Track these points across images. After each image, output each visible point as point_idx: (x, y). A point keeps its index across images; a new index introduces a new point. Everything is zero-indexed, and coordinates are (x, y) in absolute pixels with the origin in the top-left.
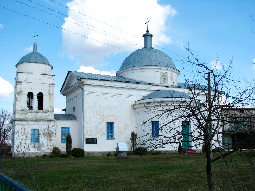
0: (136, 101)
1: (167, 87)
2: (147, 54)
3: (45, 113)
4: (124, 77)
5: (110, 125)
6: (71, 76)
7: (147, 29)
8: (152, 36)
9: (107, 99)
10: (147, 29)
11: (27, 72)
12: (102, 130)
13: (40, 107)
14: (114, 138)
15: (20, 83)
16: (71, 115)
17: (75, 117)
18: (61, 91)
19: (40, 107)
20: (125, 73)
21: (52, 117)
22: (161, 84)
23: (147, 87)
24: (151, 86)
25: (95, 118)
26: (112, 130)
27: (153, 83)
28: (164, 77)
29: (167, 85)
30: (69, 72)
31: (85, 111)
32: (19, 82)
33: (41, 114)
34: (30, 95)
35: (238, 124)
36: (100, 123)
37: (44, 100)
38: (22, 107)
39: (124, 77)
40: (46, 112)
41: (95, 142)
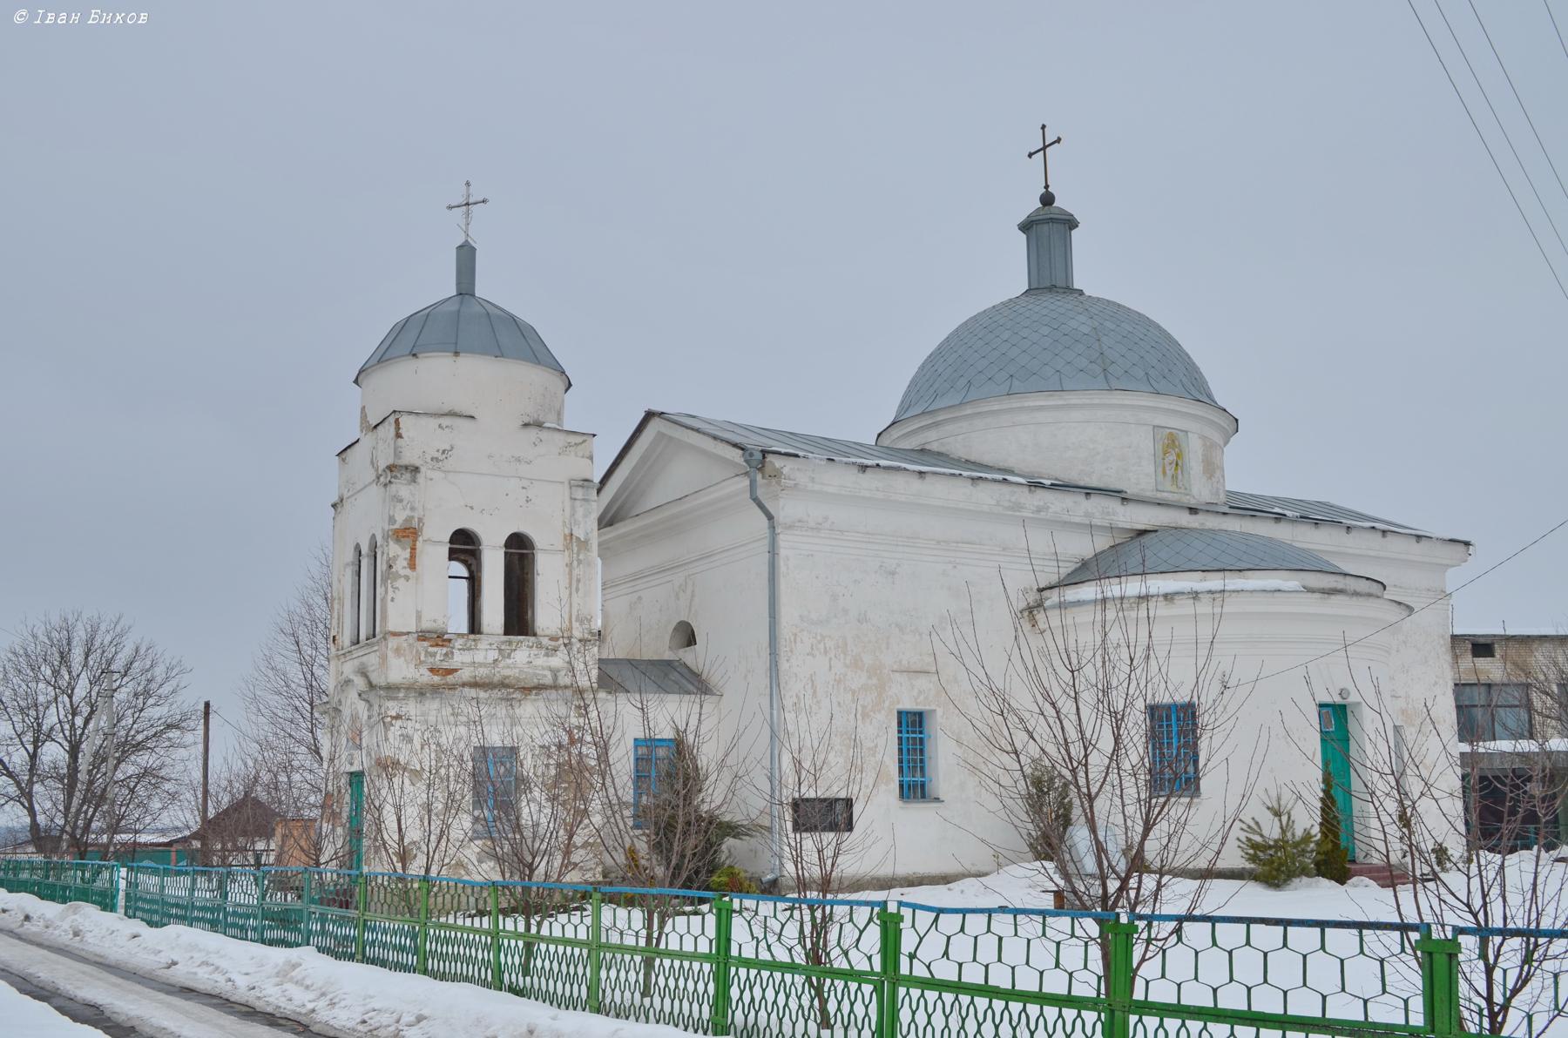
0: (1041, 590)
1: (1193, 511)
2: (1073, 324)
3: (547, 655)
4: (942, 450)
5: (913, 725)
7: (1047, 187)
8: (1071, 223)
9: (893, 573)
10: (1047, 187)
11: (446, 409)
13: (518, 620)
14: (937, 800)
15: (408, 476)
17: (697, 676)
19: (518, 620)
20: (949, 428)
22: (1159, 495)
23: (1097, 504)
24: (1113, 505)
25: (839, 682)
29: (1193, 503)
30: (649, 415)
31: (783, 642)
32: (406, 468)
33: (524, 658)
35: (441, 926)
38: (419, 617)
39: (939, 454)
41: (841, 819)
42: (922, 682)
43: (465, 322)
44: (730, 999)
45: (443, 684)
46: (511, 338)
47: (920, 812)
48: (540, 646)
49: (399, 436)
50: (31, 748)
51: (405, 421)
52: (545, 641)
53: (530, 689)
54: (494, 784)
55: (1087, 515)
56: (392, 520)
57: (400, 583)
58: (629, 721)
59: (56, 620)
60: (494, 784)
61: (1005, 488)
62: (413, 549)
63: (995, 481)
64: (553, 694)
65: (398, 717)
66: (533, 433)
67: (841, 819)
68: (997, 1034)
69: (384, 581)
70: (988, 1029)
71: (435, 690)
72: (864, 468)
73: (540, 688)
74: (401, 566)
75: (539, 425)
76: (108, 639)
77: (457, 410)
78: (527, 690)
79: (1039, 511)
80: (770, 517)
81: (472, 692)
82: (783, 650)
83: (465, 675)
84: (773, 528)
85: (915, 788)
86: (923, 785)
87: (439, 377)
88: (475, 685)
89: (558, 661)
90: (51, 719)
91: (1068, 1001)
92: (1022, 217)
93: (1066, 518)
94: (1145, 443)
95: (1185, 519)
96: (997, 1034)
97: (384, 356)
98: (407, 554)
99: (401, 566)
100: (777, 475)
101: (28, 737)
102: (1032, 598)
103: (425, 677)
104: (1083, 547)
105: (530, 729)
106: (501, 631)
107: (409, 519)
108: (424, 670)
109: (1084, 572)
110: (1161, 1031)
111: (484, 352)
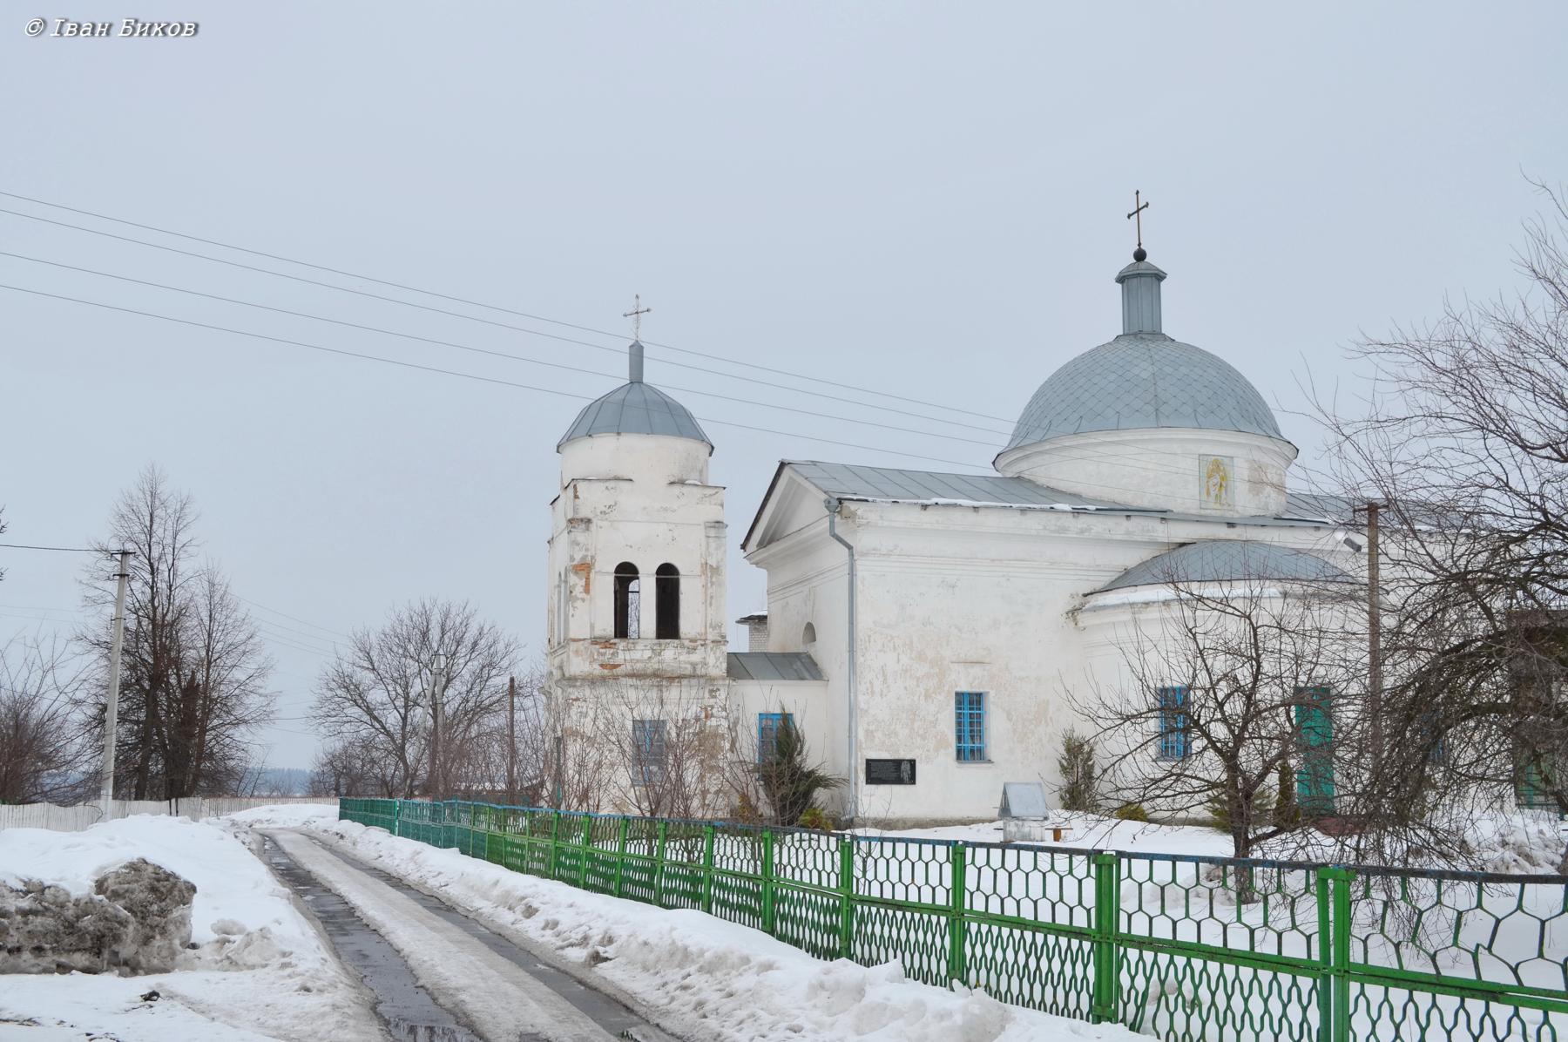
1: (1231, 525)
5: (970, 706)
6: (791, 481)
8: (1159, 277)
12: (934, 723)
13: (668, 624)
16: (797, 656)
18: (743, 547)
19: (668, 624)
21: (716, 664)
23: (1137, 525)
26: (979, 724)
27: (1165, 507)
28: (1216, 474)
29: (1231, 515)
30: (782, 465)
33: (670, 654)
34: (626, 573)
36: (927, 697)
37: (682, 597)
38: (592, 627)
40: (696, 643)
41: (906, 776)
42: (976, 670)
43: (637, 408)
44: (1119, 987)
45: (609, 676)
46: (669, 418)
47: (973, 770)
48: (683, 646)
49: (576, 497)
50: (402, 711)
51: (581, 486)
52: (687, 643)
53: (671, 679)
54: (651, 747)
55: (1128, 533)
56: (572, 558)
57: (579, 603)
58: (762, 697)
59: (418, 607)
60: (651, 747)
61: (1052, 516)
62: (588, 578)
63: (1042, 510)
64: (694, 682)
65: (577, 699)
66: (676, 489)
67: (906, 776)
68: (1397, 1036)
69: (567, 603)
70: (1385, 1031)
71: (603, 679)
72: (925, 507)
73: (681, 677)
74: (578, 591)
75: (682, 483)
76: (458, 620)
77: (620, 474)
78: (671, 679)
79: (1082, 532)
80: (850, 548)
81: (630, 681)
82: (859, 646)
83: (627, 668)
84: (852, 555)
85: (970, 748)
86: (980, 750)
87: (603, 452)
88: (626, 676)
89: (696, 657)
90: (416, 688)
91: (1278, 963)
92: (1116, 274)
93: (1107, 536)
94: (1190, 465)
95: (1223, 532)
96: (1397, 1036)
97: (570, 438)
98: (583, 582)
99: (578, 591)
100: (851, 516)
101: (400, 702)
102: (1077, 603)
103: (597, 670)
104: (1131, 558)
105: (680, 705)
106: (653, 634)
107: (584, 557)
108: (596, 666)
109: (1126, 579)
110: (1546, 1029)
111: (638, 431)
